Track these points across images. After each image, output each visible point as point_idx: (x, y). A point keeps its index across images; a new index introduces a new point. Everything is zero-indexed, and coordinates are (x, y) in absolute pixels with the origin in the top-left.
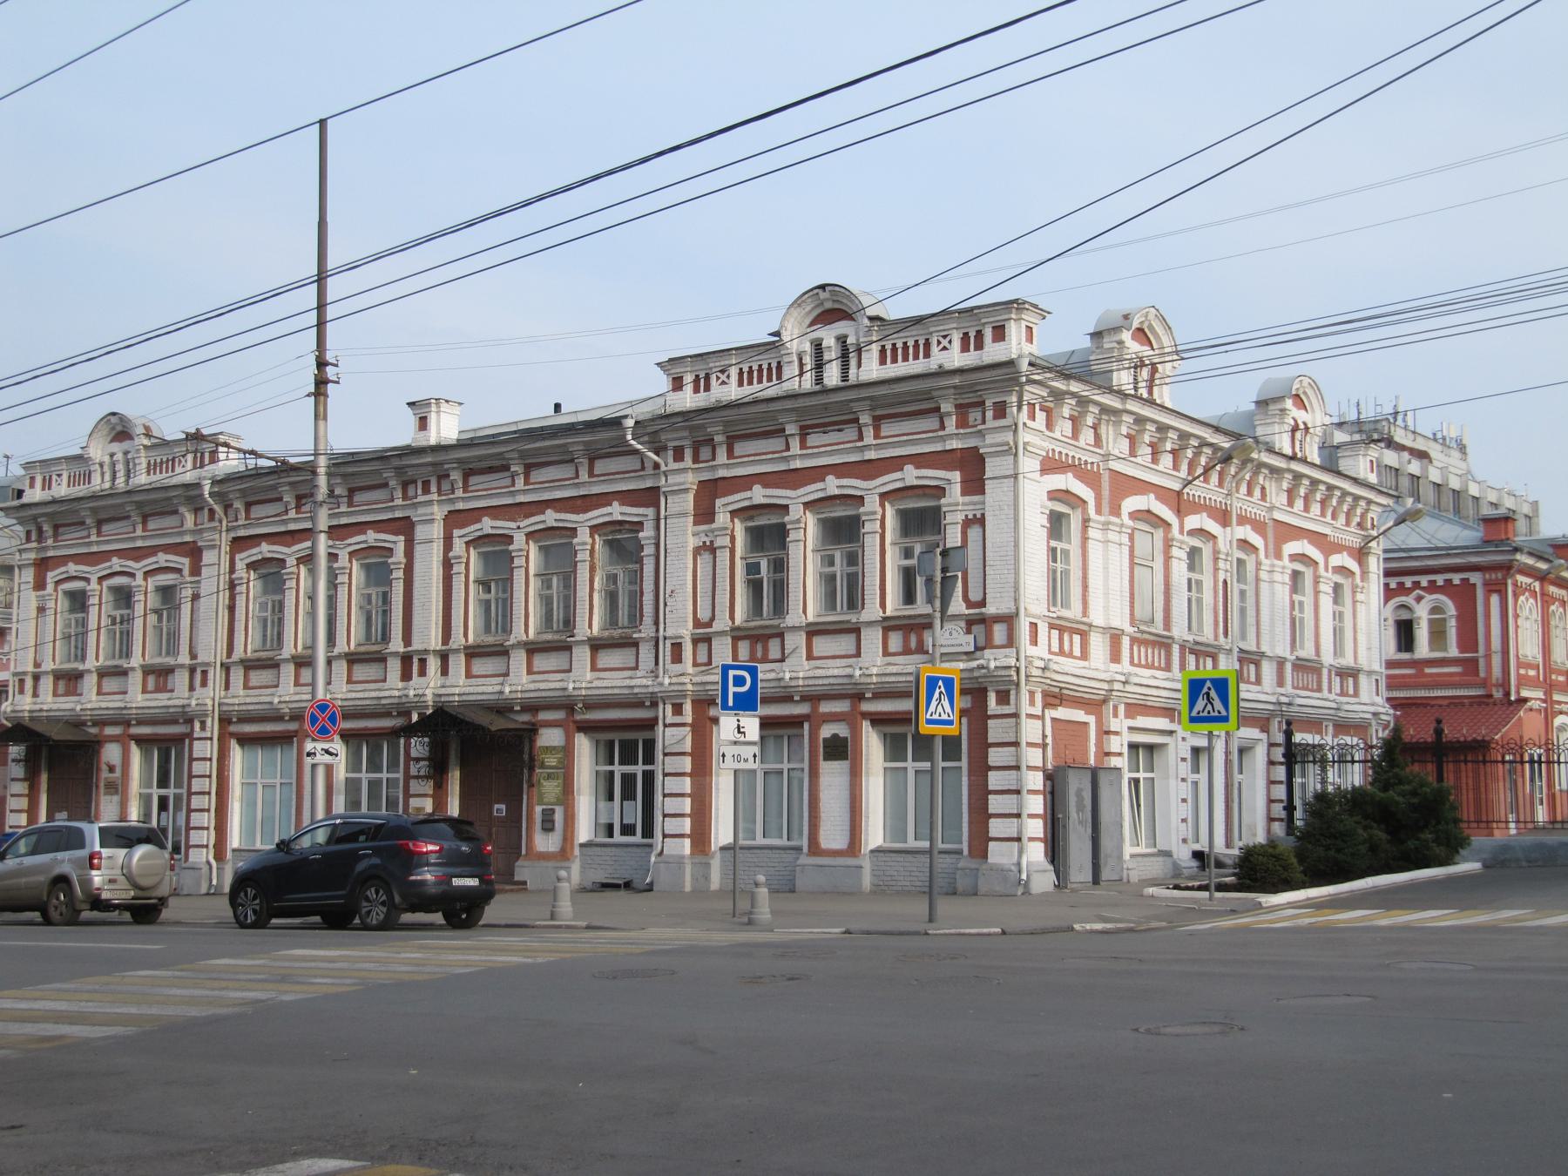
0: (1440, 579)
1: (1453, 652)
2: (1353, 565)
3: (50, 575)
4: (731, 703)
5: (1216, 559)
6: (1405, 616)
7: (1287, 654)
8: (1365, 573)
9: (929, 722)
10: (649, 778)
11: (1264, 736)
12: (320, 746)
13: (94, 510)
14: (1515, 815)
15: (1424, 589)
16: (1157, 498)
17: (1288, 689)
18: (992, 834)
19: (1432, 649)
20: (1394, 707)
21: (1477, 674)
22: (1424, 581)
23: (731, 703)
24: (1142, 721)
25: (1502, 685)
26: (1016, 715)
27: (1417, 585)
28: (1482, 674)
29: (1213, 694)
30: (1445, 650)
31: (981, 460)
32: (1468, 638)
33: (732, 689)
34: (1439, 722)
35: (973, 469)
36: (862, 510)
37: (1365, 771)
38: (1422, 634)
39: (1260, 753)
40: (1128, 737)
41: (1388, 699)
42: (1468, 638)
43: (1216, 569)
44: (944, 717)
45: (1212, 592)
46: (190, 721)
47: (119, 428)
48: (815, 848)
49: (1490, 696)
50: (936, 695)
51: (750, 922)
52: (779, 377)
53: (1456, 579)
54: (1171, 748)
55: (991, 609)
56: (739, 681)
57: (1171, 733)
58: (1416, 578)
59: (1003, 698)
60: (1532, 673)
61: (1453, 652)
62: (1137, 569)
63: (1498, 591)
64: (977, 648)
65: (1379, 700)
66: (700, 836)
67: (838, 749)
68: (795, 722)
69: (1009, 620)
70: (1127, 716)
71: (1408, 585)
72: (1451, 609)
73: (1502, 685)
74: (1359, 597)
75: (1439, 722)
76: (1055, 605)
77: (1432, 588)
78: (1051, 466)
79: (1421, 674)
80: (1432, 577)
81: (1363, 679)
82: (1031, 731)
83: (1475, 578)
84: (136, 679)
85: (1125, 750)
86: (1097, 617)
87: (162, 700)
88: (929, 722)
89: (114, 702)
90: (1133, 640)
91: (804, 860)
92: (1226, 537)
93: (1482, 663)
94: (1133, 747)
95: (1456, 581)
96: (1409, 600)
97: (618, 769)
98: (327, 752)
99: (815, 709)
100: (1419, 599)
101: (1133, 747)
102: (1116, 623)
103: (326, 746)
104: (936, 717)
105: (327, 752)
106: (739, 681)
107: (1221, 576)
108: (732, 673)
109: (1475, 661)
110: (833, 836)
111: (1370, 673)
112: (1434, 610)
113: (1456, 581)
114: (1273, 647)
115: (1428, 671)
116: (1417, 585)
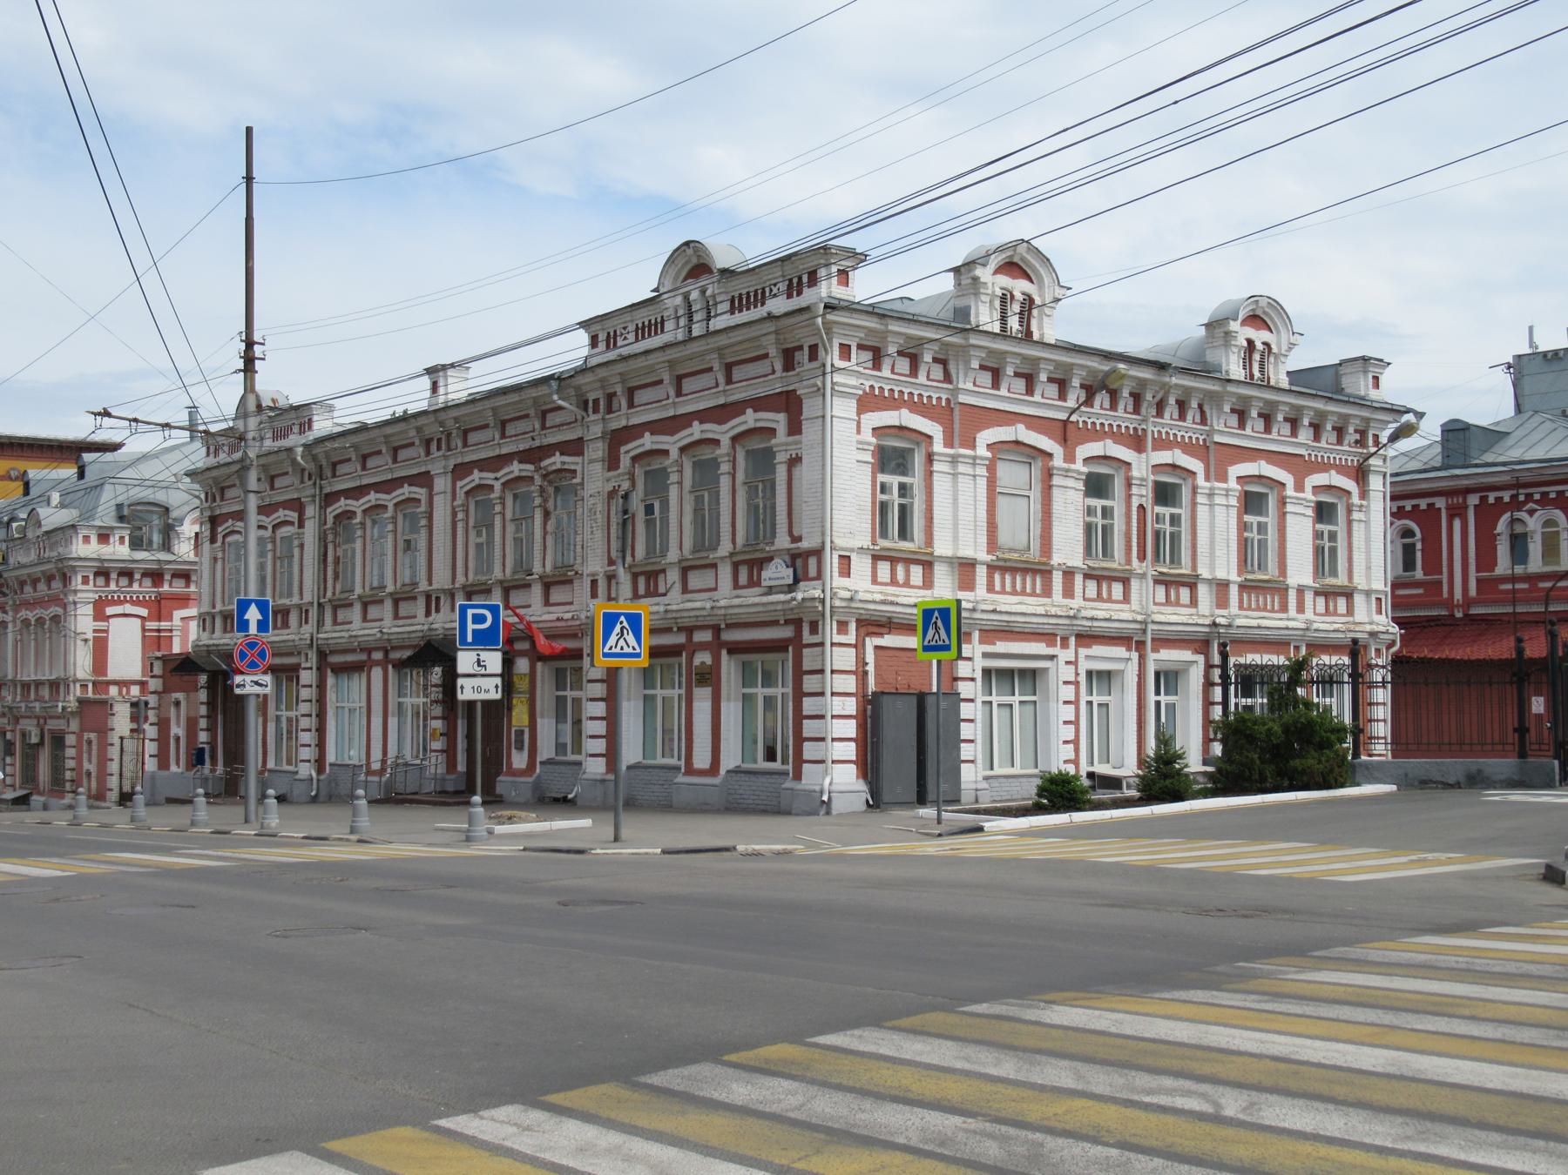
0: (1553, 491)
1: (1419, 574)
2: (1349, 484)
3: (623, 449)
4: (470, 639)
5: (1129, 485)
6: (1518, 529)
7: (1234, 577)
8: (1364, 494)
9: (605, 655)
10: (577, 702)
11: (1201, 659)
12: (248, 679)
13: (672, 364)
15: (1536, 502)
16: (1028, 428)
17: (1234, 608)
19: (1545, 563)
23: (470, 639)
24: (1001, 647)
26: (822, 644)
28: (1445, 595)
29: (940, 623)
30: (1558, 563)
31: (798, 402)
33: (471, 626)
34: (1519, 640)
35: (790, 404)
36: (773, 441)
38: (1535, 548)
39: (1196, 677)
40: (980, 663)
41: (1394, 620)
43: (1129, 496)
44: (626, 650)
45: (1123, 520)
46: (797, 623)
47: (694, 261)
48: (690, 771)
49: (1452, 615)
50: (617, 629)
51: (468, 839)
52: (732, 301)
53: (1423, 504)
54: (1052, 673)
55: (805, 545)
56: (479, 619)
57: (1052, 657)
59: (814, 628)
61: (1419, 574)
62: (1001, 501)
64: (797, 580)
65: (1382, 619)
66: (612, 755)
67: (709, 677)
68: (674, 651)
69: (818, 553)
70: (981, 642)
74: (1355, 516)
76: (884, 534)
77: (1545, 501)
78: (868, 402)
79: (1533, 589)
81: (1358, 599)
82: (844, 658)
83: (1440, 503)
84: (725, 572)
85: (978, 675)
86: (1359, 581)
87: (752, 597)
88: (605, 655)
89: (700, 603)
90: (991, 568)
91: (681, 779)
92: (1142, 465)
94: (987, 672)
95: (1423, 506)
97: (760, 692)
98: (257, 683)
99: (690, 638)
100: (1531, 512)
101: (987, 672)
102: (967, 552)
103: (255, 678)
104: (618, 650)
105: (257, 683)
106: (479, 619)
107: (1135, 502)
108: (470, 612)
110: (702, 759)
111: (1368, 593)
112: (1549, 523)
113: (1423, 506)
114: (1212, 567)
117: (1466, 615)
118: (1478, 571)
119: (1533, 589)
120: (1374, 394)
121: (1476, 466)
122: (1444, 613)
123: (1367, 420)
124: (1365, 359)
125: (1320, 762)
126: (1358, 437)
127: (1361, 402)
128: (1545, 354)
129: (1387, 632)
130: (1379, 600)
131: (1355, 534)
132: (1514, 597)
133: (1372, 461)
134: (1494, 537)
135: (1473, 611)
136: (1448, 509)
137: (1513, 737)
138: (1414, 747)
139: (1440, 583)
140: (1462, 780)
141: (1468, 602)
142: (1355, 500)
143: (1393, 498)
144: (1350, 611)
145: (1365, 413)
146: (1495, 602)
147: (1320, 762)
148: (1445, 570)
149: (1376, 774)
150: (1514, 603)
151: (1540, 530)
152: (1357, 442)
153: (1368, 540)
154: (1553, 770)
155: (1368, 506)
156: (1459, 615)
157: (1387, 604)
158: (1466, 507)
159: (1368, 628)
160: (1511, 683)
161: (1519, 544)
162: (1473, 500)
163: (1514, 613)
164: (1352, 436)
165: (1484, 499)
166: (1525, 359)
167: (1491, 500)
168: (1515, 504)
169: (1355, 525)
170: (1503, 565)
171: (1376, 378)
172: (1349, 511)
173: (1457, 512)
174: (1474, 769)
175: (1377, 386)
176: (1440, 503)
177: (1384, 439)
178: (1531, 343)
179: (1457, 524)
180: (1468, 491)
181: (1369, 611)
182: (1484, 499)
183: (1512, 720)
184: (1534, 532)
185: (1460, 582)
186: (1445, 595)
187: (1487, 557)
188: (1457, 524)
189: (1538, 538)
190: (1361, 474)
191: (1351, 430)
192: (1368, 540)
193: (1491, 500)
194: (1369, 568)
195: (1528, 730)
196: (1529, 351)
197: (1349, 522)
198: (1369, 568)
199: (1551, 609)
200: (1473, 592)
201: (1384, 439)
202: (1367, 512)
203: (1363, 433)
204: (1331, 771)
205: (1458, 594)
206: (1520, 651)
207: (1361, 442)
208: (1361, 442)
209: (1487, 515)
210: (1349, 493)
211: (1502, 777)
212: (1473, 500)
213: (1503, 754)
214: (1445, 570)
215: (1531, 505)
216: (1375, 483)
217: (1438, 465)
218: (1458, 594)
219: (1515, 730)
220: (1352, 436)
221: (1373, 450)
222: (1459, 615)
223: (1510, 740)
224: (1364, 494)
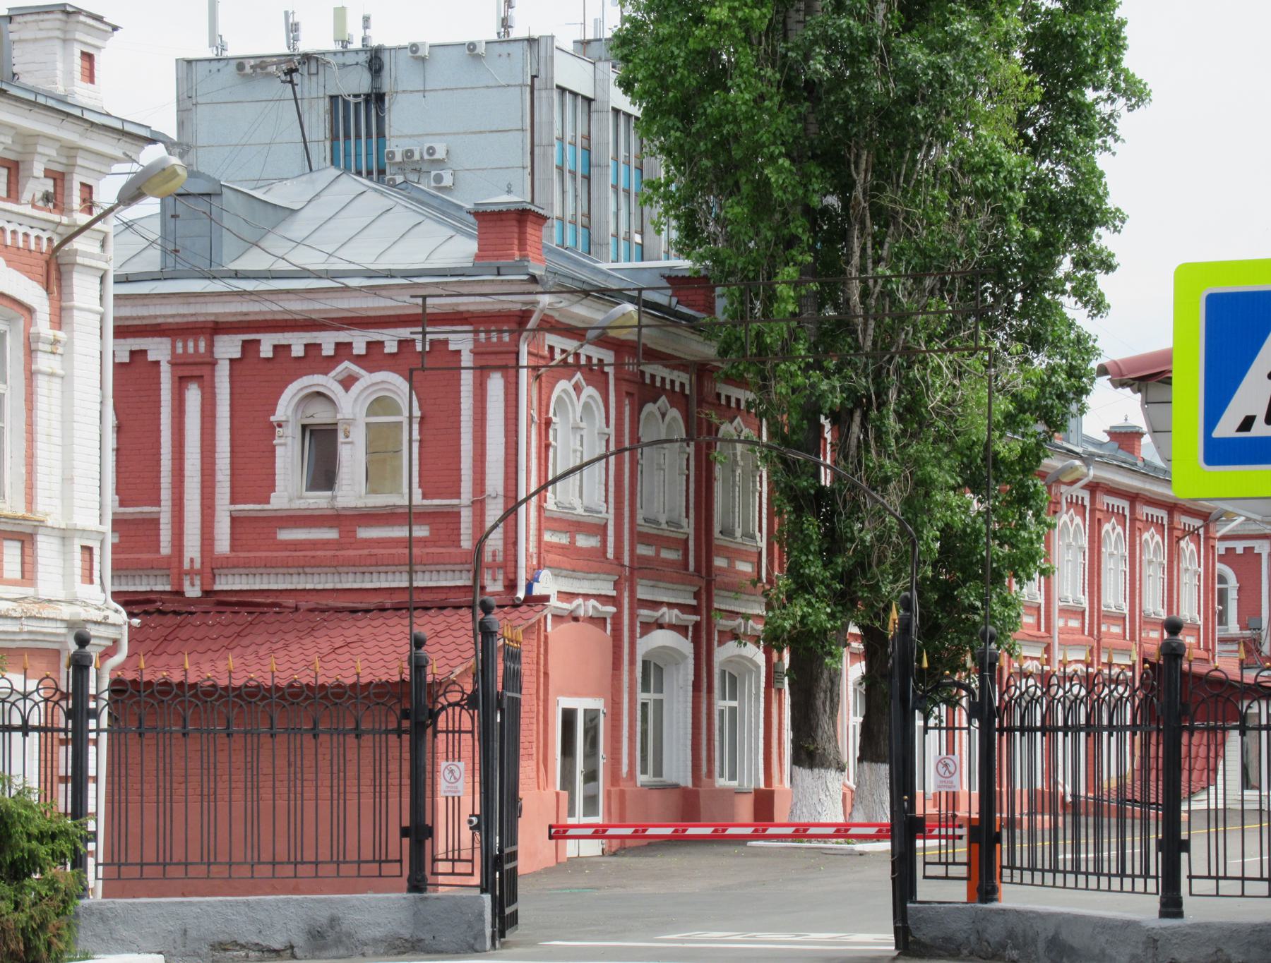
0: (390, 339)
2: (31, 292)
6: (320, 415)
8: (60, 317)
14: (803, 773)
15: (358, 360)
18: (965, 868)
20: (125, 604)
21: (456, 542)
22: (359, 340)
25: (503, 566)
27: (343, 349)
28: (165, 549)
32: (440, 469)
34: (418, 643)
37: (1145, 745)
38: (352, 457)
41: (115, 595)
42: (440, 469)
49: (179, 593)
53: (1239, 547)
58: (343, 337)
60: (745, 567)
63: (502, 368)
71: (328, 350)
72: (1233, 583)
73: (503, 566)
74: (44, 362)
75: (418, 643)
77: (374, 358)
79: (348, 541)
80: (375, 335)
81: (46, 547)
83: (462, 342)
86: (49, 508)
93: (466, 516)
95: (1240, 551)
96: (327, 383)
100: (348, 382)
109: (453, 516)
111: (65, 535)
112: (381, 404)
113: (1240, 551)
115: (365, 533)
116: (343, 349)
117: (207, 593)
118: (233, 501)
119: (348, 541)
120: (83, 94)
121: (237, 275)
122: (163, 586)
123: (71, 151)
124: (69, 13)
125: (17, 906)
126: (49, 186)
127: (61, 110)
128: (240, 64)
129: (103, 623)
130: (88, 550)
131: (42, 403)
132: (304, 558)
133: (78, 244)
134: (272, 428)
135: (222, 584)
136: (174, 364)
137: (399, 847)
138: (266, 870)
139: (155, 522)
140: (299, 940)
141: (212, 565)
142: (43, 326)
143: (122, 331)
144: (28, 574)
145: (70, 134)
146: (268, 566)
147: (17, 906)
148: (166, 494)
149: (123, 932)
150: (411, 566)
151: (362, 419)
152: (47, 198)
153: (67, 420)
154: (481, 915)
155: (70, 344)
156: (192, 591)
157: (104, 562)
158: (213, 363)
159: (66, 612)
160: (399, 732)
161: (322, 442)
162: (228, 347)
163: (410, 590)
164: (37, 185)
165: (250, 347)
166: (201, 69)
167: (266, 351)
168: (314, 360)
169: (42, 383)
170: (289, 488)
171: (88, 57)
172: (30, 352)
173: (193, 371)
174: (322, 916)
175: (90, 77)
176: (462, 342)
177: (107, 193)
178: (215, 39)
179: (193, 396)
180: (218, 328)
181: (66, 575)
182: (250, 347)
183: (399, 813)
184: (350, 422)
185: (198, 526)
186: (165, 549)
187: (253, 473)
188: (193, 396)
189: (359, 436)
190: (54, 270)
191: (38, 169)
192: (67, 420)
193: (266, 351)
194: (68, 480)
195: (430, 832)
196: (210, 54)
197: (30, 375)
198: (68, 480)
199: (418, 583)
200: (223, 544)
201: (107, 193)
202: (67, 357)
203: (59, 178)
204: (43, 926)
205: (192, 549)
206: (419, 666)
207: (54, 200)
208: (54, 200)
209: (259, 380)
210: (30, 310)
211: (377, 933)
212: (228, 347)
213: (377, 881)
214: (166, 494)
215: (346, 366)
216: (84, 291)
217: (156, 267)
218: (192, 549)
219: (405, 832)
220: (37, 185)
221: (83, 219)
222: (192, 591)
223: (394, 855)
224: (60, 317)
